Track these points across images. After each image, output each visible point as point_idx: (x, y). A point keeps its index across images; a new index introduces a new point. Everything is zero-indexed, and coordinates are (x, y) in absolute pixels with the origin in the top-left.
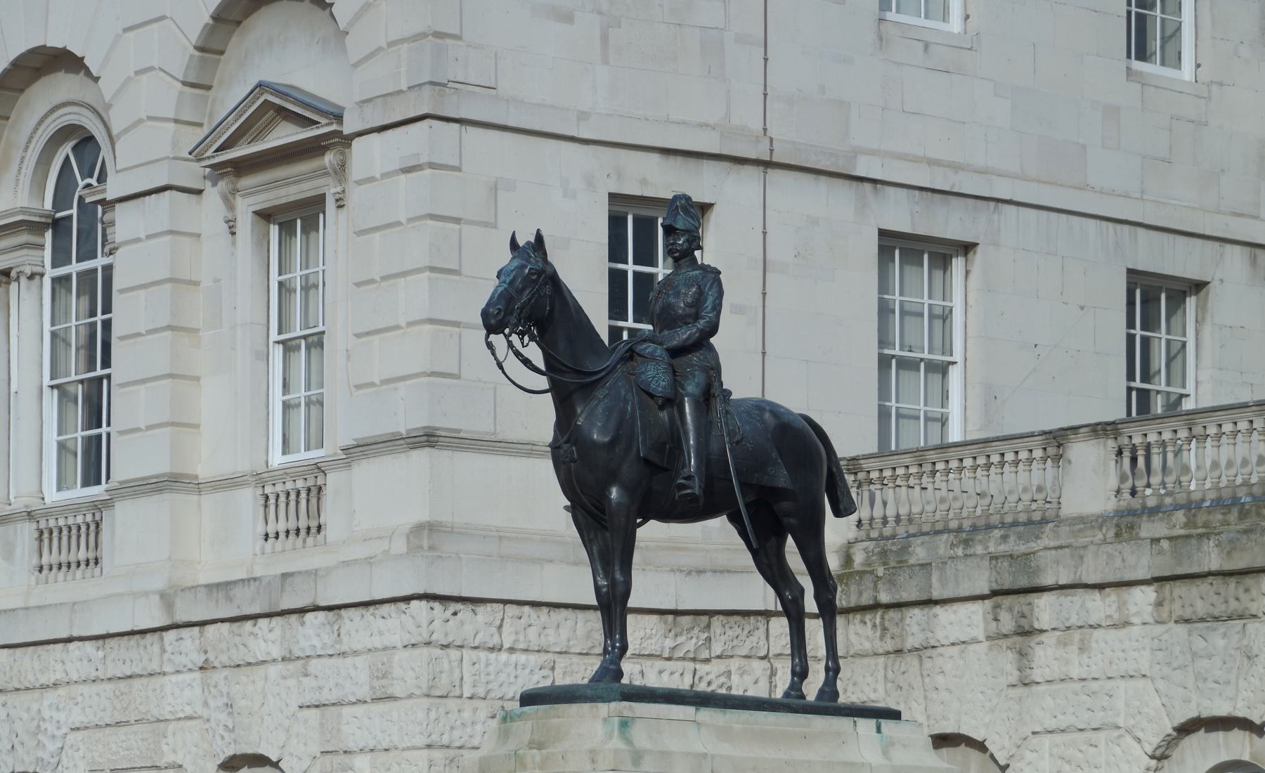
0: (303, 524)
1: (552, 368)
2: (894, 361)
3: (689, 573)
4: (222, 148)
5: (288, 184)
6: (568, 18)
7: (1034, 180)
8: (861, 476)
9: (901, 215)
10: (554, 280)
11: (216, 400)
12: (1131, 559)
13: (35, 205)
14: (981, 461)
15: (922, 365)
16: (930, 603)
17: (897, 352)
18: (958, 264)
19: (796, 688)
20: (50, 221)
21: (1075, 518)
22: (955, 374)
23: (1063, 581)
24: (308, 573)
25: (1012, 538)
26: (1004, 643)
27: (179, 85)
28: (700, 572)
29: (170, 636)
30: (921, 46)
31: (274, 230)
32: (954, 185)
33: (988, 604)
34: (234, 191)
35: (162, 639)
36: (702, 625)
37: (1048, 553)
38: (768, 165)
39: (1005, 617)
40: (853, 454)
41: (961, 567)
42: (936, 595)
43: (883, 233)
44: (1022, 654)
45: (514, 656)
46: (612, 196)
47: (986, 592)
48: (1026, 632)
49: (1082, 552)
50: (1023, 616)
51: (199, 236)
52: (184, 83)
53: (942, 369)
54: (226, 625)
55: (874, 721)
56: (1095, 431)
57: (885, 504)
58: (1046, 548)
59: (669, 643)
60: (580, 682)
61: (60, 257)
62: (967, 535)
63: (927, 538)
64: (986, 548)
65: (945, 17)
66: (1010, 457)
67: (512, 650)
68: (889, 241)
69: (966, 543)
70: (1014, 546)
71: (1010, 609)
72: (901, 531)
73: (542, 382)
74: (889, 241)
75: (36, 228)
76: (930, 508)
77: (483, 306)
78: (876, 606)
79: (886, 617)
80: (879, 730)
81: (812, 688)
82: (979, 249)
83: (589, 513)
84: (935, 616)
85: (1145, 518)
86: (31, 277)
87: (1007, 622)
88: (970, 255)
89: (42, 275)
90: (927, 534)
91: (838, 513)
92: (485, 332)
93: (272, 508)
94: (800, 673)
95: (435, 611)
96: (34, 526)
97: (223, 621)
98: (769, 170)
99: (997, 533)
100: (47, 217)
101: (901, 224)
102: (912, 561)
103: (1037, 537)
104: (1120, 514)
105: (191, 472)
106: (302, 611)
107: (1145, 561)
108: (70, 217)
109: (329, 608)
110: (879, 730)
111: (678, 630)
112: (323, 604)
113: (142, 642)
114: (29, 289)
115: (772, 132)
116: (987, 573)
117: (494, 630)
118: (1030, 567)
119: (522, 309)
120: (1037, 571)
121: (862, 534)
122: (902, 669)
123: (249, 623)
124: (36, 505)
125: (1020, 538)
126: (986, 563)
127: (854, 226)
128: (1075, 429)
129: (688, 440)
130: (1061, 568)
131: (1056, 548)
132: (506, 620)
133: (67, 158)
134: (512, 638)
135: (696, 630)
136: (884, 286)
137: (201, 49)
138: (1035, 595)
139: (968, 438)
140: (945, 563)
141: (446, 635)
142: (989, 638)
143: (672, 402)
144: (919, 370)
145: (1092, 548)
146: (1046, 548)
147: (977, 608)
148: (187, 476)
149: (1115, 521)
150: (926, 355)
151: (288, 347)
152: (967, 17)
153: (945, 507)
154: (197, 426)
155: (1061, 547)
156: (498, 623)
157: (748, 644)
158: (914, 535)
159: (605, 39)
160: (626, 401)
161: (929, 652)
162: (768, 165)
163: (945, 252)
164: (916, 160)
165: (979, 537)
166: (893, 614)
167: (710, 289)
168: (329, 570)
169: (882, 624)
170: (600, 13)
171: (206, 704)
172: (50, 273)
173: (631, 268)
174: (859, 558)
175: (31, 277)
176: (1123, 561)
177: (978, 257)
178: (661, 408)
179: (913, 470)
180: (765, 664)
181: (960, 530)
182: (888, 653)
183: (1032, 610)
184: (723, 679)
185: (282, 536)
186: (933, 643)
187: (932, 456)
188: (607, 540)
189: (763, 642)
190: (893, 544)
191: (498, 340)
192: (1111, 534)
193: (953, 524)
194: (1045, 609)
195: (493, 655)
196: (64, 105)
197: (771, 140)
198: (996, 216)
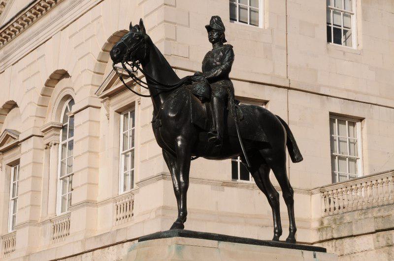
8: (325, 193)
10: (149, 41)
11: (103, 176)
14: (369, 183)
15: (347, 159)
17: (338, 154)
18: (358, 124)
19: (276, 238)
20: (61, 127)
22: (359, 162)
24: (124, 228)
25: (382, 210)
26: (382, 250)
27: (93, 73)
30: (342, 53)
31: (122, 116)
34: (109, 105)
35: (81, 257)
38: (289, 88)
40: (322, 186)
43: (331, 114)
44: (389, 254)
47: (374, 231)
50: (389, 239)
51: (99, 122)
52: (94, 72)
53: (355, 160)
55: (313, 252)
57: (334, 203)
61: (64, 137)
62: (365, 211)
65: (352, 46)
66: (379, 181)
68: (333, 116)
71: (383, 237)
74: (333, 116)
75: (58, 128)
76: (351, 202)
79: (337, 243)
80: (315, 256)
81: (284, 237)
82: (365, 120)
83: (170, 152)
86: (55, 144)
89: (59, 144)
90: (350, 212)
91: (294, 161)
93: (119, 209)
94: (278, 232)
96: (52, 224)
97: (99, 248)
98: (289, 90)
99: (376, 209)
101: (338, 110)
102: (345, 222)
106: (123, 242)
108: (66, 126)
110: (315, 256)
115: (290, 77)
118: (390, 220)
119: (131, 52)
121: (327, 214)
123: (107, 248)
124: (53, 217)
127: (321, 111)
129: (215, 116)
133: (67, 107)
136: (332, 132)
139: (365, 175)
140: (357, 221)
143: (207, 99)
144: (346, 160)
147: (371, 237)
148: (93, 201)
150: (348, 156)
151: (126, 155)
152: (358, 45)
153: (356, 201)
154: (97, 184)
160: (185, 99)
162: (289, 88)
163: (353, 121)
166: (339, 241)
167: (227, 53)
169: (335, 245)
172: (61, 143)
174: (326, 223)
175: (55, 144)
177: (365, 122)
178: (203, 102)
179: (344, 189)
181: (362, 209)
185: (122, 218)
186: (354, 251)
187: (351, 183)
188: (178, 161)
193: (360, 208)
196: (65, 89)
197: (290, 80)
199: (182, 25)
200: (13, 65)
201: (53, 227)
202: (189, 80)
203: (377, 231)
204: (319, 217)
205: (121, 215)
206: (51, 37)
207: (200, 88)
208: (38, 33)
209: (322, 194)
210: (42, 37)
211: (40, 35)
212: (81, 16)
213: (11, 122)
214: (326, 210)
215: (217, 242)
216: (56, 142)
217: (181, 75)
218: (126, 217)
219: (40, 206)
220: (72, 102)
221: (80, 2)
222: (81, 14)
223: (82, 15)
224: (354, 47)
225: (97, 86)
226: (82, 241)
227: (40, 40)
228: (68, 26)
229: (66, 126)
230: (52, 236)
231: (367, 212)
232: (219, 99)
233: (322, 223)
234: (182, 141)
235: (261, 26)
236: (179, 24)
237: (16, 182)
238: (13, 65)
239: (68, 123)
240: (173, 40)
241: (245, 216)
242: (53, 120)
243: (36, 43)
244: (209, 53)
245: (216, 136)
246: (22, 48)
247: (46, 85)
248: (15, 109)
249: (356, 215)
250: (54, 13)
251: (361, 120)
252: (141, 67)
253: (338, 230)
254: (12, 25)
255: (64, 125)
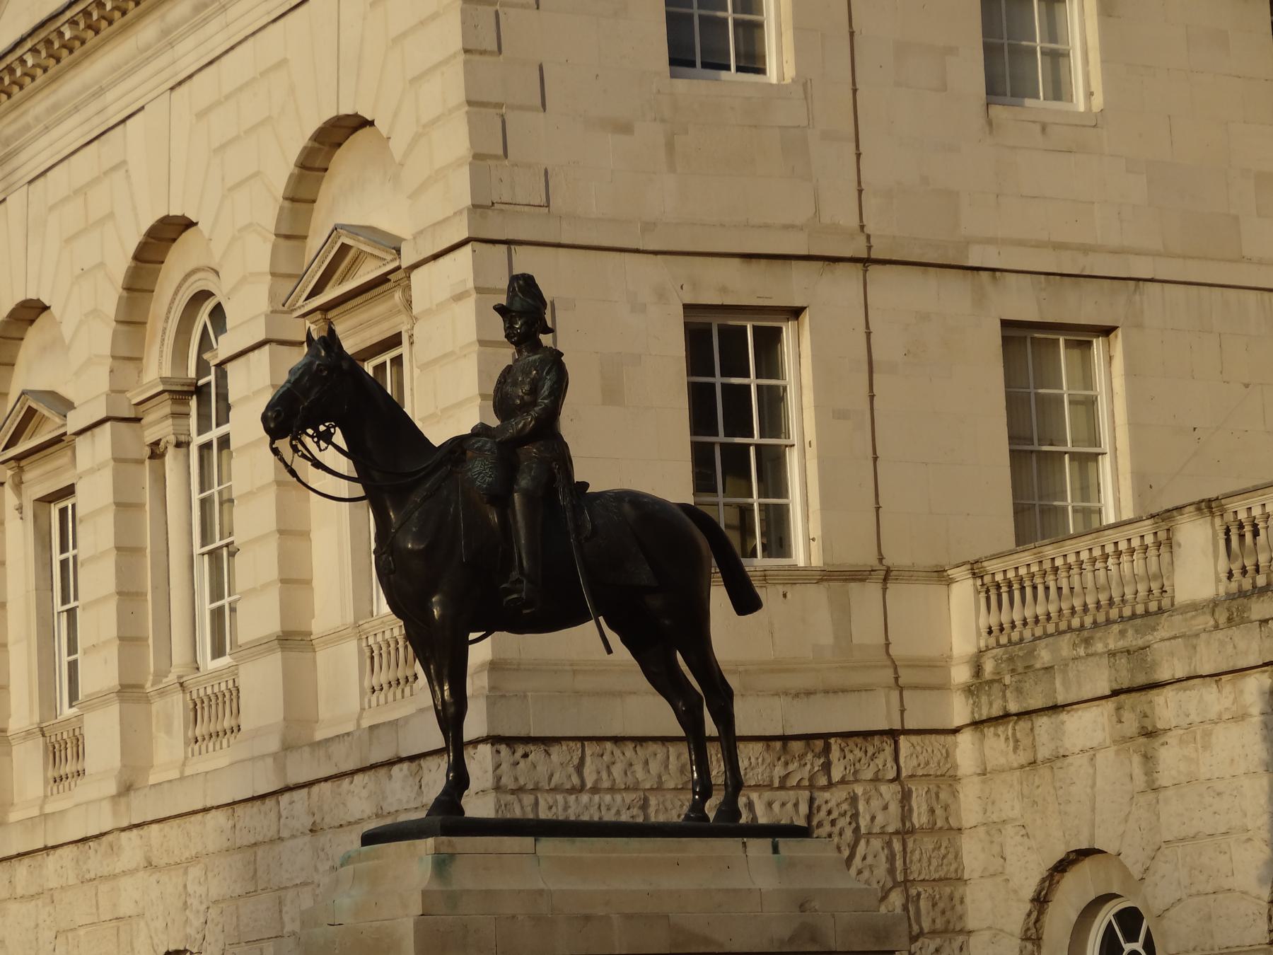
0: (400, 674)
1: (363, 476)
2: (1067, 456)
3: (797, 695)
4: (314, 293)
5: (370, 326)
6: (625, 128)
7: (1179, 257)
9: (1025, 305)
12: (1242, 645)
13: (180, 374)
16: (1055, 708)
19: (697, 807)
20: (192, 389)
21: (1188, 606)
22: (1105, 464)
23: (1179, 675)
25: (1130, 632)
28: (809, 693)
29: (285, 799)
30: (1038, 128)
32: (1084, 268)
33: (1110, 705)
35: (278, 803)
36: (817, 750)
37: (1162, 644)
38: (866, 262)
39: (1127, 715)
40: (976, 558)
41: (1082, 668)
42: (1061, 699)
43: (1005, 324)
44: (1148, 758)
45: (597, 798)
46: (688, 308)
48: (1150, 733)
49: (1194, 641)
54: (329, 784)
55: (769, 840)
56: (1199, 509)
58: (1162, 640)
59: (779, 771)
60: (675, 819)
61: (203, 427)
63: (1050, 639)
64: (1106, 645)
67: (595, 790)
68: (1014, 331)
69: (1087, 642)
70: (1132, 640)
71: (1133, 709)
72: (1027, 634)
73: (359, 490)
74: (1014, 331)
77: (263, 410)
78: (1006, 716)
80: (776, 850)
82: (1119, 332)
84: (1063, 723)
85: (1254, 599)
87: (1131, 724)
88: (1112, 336)
89: (188, 444)
90: (1052, 635)
92: (268, 438)
95: (503, 754)
97: (326, 779)
99: (1116, 628)
100: (189, 385)
102: (1038, 666)
103: (1154, 629)
104: (1231, 597)
105: (303, 629)
106: (390, 763)
107: (1255, 646)
108: (209, 384)
109: (412, 759)
110: (776, 850)
111: (788, 757)
112: (404, 755)
113: (263, 808)
114: (175, 458)
116: (1106, 673)
117: (571, 770)
120: (1154, 666)
122: (1037, 783)
125: (1137, 631)
126: (1105, 660)
128: (1179, 509)
130: (1176, 661)
131: (1169, 639)
132: (588, 759)
133: (205, 325)
134: (594, 777)
135: (810, 756)
137: (293, 200)
138: (1155, 692)
140: (1067, 665)
141: (516, 779)
142: (1115, 742)
143: (501, 499)
145: (1204, 636)
146: (1162, 640)
149: (1226, 605)
155: (1175, 637)
156: (576, 761)
157: (873, 769)
158: (1040, 638)
159: (670, 146)
161: (1058, 764)
164: (1039, 245)
165: (1099, 635)
168: (406, 719)
169: (1014, 734)
170: (663, 121)
171: (316, 869)
172: (197, 440)
173: (718, 380)
174: (989, 667)
176: (1235, 647)
177: (806, 318)
180: (895, 787)
182: (1022, 767)
183: (1153, 709)
184: (845, 807)
186: (1062, 752)
189: (890, 763)
190: (1020, 649)
191: (284, 445)
192: (1222, 620)
194: (1166, 706)
195: (572, 798)
197: (868, 237)
198: (1137, 297)
199: (521, 108)
200: (30, 182)
201: (191, 706)
202: (458, 445)
203: (1115, 693)
204: (971, 649)
205: (383, 677)
206: (143, 108)
207: (480, 471)
208: (101, 92)
209: (979, 582)
210: (115, 104)
211: (110, 96)
212: (227, 52)
213: (34, 370)
214: (990, 628)
215: (530, 840)
216: (183, 438)
217: (437, 435)
218: (399, 683)
219: (147, 639)
220: (218, 314)
221: (224, 8)
222: (228, 46)
223: (232, 48)
224: (1080, 103)
225: (290, 276)
226: (275, 756)
227: (111, 110)
228: (190, 77)
229: (209, 384)
230: (190, 734)
231: (1092, 638)
232: (529, 497)
233: (978, 671)
234: (443, 605)
235: (772, 74)
236: (512, 107)
237: (70, 554)
238: (30, 182)
239: (212, 378)
240: (496, 157)
241: (741, 668)
242: (167, 372)
243: (96, 121)
244: (508, 370)
245: (519, 591)
246: (55, 133)
247: (136, 257)
248: (42, 319)
249: (1065, 646)
250: (147, 32)
251: (1107, 331)
252: (338, 438)
253: (1019, 691)
254: (22, 61)
255: (201, 382)
